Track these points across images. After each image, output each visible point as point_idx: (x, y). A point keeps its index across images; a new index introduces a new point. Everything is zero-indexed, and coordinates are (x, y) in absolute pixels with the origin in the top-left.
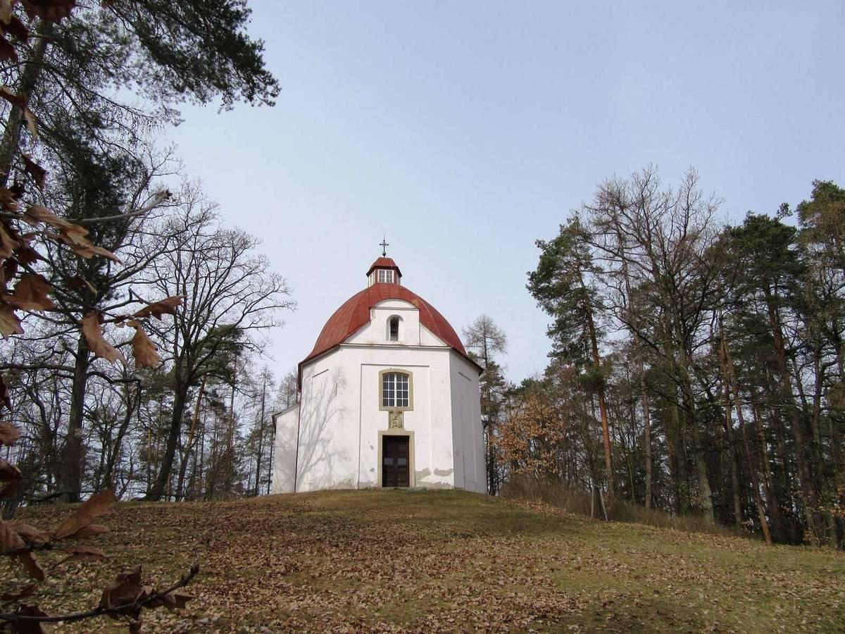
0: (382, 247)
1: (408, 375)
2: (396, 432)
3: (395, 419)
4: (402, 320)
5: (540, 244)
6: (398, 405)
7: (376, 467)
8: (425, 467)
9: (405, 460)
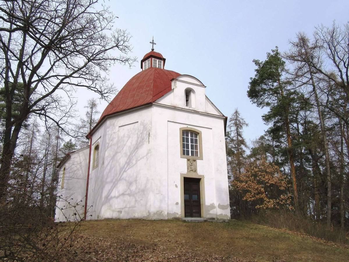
0: (151, 45)
1: (198, 133)
2: (192, 175)
3: (192, 165)
4: (194, 92)
5: (256, 62)
6: (191, 155)
7: (179, 202)
8: (212, 203)
9: (196, 196)
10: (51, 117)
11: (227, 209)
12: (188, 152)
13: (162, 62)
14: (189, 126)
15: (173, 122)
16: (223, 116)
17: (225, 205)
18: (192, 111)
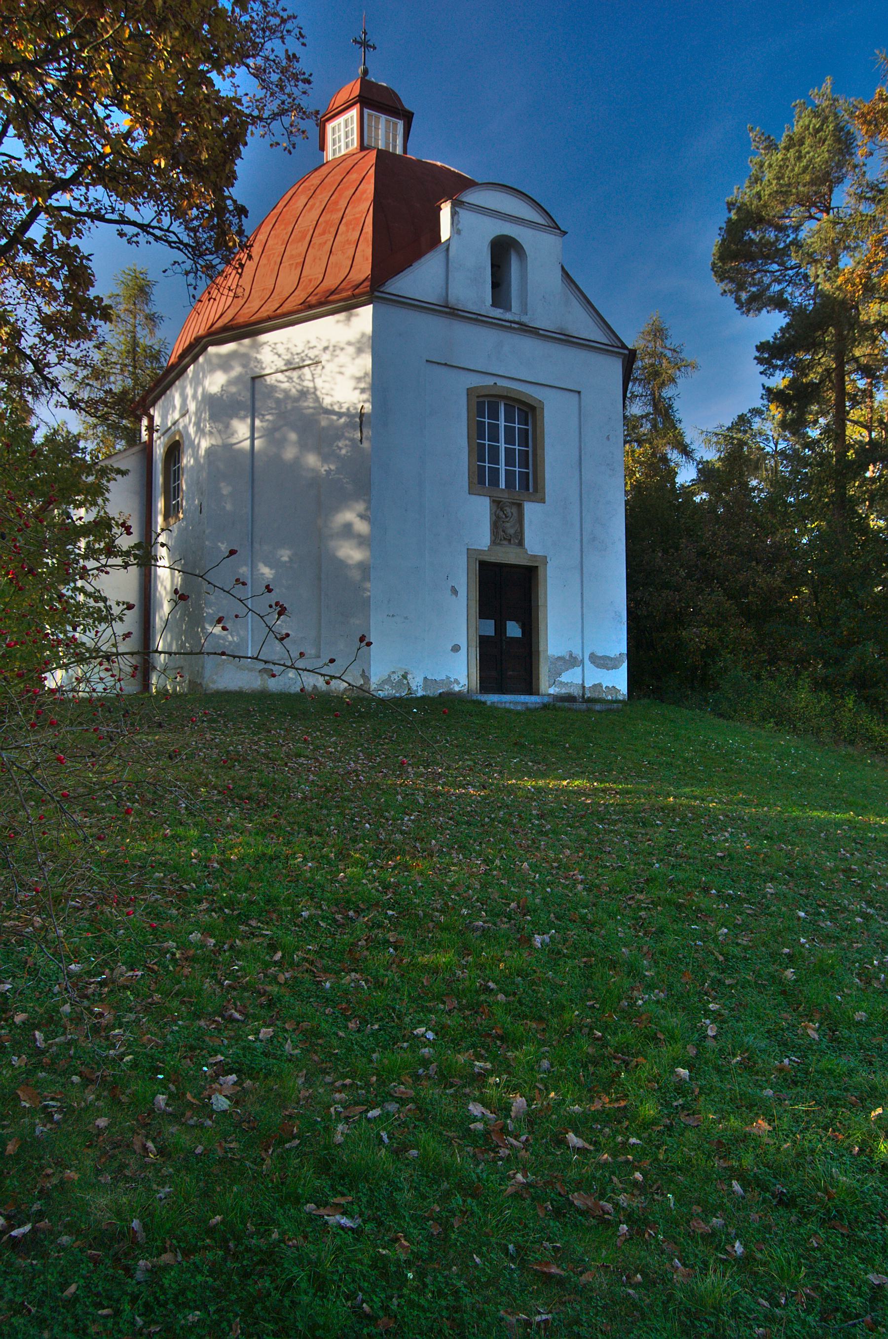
1: (533, 409)
2: (509, 556)
10: (471, 307)
11: (615, 667)
12: (495, 472)
13: (400, 125)
14: (502, 383)
15: (446, 364)
16: (624, 347)
17: (612, 656)
18: (513, 325)
